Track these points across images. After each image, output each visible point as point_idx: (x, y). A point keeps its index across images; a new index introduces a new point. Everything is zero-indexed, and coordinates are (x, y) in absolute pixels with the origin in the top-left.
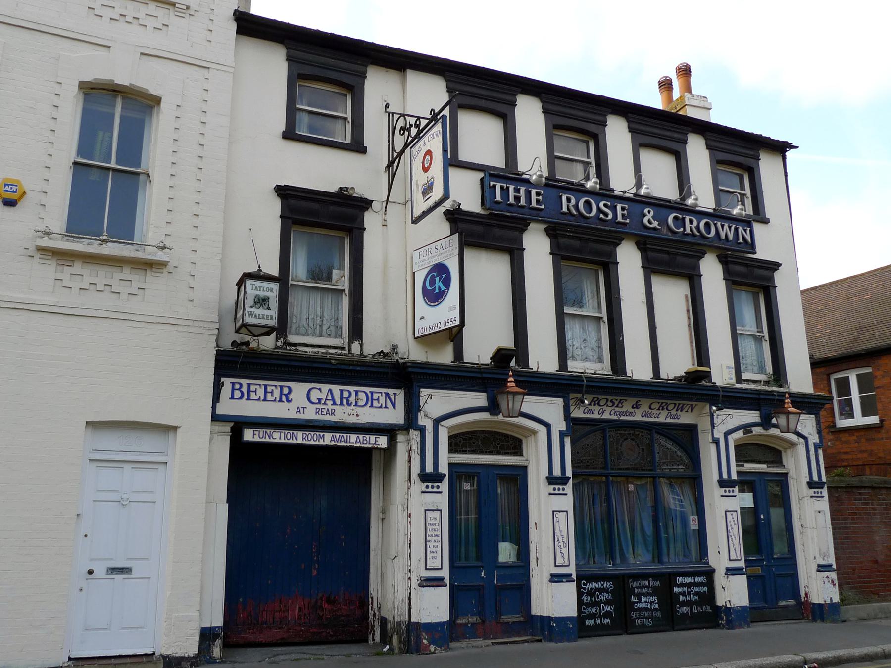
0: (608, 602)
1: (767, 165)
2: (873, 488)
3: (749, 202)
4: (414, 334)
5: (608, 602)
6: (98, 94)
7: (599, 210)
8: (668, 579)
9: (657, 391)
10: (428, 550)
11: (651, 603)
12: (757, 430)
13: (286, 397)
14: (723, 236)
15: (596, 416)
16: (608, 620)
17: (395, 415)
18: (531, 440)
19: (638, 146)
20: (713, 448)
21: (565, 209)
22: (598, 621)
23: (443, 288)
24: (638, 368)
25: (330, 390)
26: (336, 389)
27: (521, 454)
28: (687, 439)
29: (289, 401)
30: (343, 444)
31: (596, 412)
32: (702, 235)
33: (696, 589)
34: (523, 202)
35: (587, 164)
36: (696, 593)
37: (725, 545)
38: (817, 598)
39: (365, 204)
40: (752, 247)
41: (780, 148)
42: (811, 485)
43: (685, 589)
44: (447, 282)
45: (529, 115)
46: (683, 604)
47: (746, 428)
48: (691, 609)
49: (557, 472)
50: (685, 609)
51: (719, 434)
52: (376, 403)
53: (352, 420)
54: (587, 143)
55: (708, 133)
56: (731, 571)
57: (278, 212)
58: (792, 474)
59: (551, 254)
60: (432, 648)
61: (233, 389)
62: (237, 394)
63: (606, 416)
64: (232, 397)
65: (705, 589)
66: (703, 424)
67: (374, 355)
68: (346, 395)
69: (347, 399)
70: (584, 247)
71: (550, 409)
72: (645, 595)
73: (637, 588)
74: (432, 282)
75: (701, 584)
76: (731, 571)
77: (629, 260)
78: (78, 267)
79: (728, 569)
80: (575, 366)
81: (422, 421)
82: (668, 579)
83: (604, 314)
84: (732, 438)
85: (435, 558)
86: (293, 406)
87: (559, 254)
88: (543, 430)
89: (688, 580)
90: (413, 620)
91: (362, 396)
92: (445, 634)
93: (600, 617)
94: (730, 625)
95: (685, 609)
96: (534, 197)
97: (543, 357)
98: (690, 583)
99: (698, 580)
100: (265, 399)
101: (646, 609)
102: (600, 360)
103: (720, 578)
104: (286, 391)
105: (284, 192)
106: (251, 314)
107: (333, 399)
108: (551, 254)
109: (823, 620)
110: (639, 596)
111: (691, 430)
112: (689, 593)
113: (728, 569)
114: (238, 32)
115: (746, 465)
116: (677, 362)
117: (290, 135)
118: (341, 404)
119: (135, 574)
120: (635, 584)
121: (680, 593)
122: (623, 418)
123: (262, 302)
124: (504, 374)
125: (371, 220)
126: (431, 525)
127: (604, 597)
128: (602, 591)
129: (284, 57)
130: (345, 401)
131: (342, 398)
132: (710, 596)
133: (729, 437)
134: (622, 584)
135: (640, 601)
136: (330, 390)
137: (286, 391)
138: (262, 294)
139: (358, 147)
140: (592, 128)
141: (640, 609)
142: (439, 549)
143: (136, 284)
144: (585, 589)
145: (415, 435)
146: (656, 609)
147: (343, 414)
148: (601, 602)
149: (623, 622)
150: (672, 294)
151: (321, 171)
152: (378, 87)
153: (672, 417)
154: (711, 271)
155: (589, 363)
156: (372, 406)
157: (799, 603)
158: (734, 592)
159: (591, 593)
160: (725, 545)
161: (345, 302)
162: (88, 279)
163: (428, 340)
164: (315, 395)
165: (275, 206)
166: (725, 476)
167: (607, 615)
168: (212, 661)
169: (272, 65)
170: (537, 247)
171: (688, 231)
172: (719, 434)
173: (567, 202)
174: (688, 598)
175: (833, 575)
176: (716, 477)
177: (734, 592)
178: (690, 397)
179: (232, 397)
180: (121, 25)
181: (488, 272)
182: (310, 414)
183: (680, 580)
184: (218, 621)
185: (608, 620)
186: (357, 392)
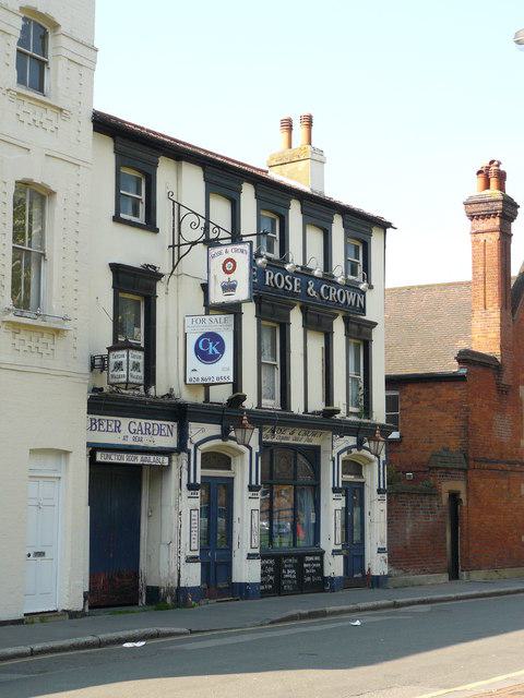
0: (272, 574)
1: (376, 239)
4: (185, 381)
6: (24, 186)
8: (301, 557)
9: (308, 422)
12: (354, 451)
13: (118, 429)
17: (170, 441)
18: (239, 458)
21: (267, 283)
26: (143, 421)
27: (230, 469)
28: (314, 455)
37: (331, 536)
38: (376, 572)
39: (159, 276)
40: (363, 310)
41: (384, 226)
44: (221, 348)
46: (308, 575)
47: (348, 449)
49: (254, 483)
50: (309, 579)
53: (151, 445)
55: (118, 138)
56: (335, 552)
58: (368, 483)
66: (325, 446)
67: (163, 397)
74: (206, 345)
76: (335, 552)
77: (296, 318)
78: (23, 335)
79: (334, 551)
81: (190, 447)
82: (301, 557)
83: (278, 363)
86: (121, 435)
88: (247, 451)
89: (311, 558)
90: (182, 585)
91: (156, 427)
92: (199, 594)
94: (333, 590)
95: (309, 579)
102: (273, 398)
103: (328, 558)
105: (117, 269)
106: (112, 376)
109: (378, 587)
111: (316, 451)
113: (334, 551)
114: (94, 130)
116: (317, 404)
117: (117, 219)
119: (47, 556)
124: (230, 415)
125: (160, 288)
129: (112, 150)
130: (148, 431)
132: (320, 571)
134: (278, 558)
139: (150, 225)
145: (184, 455)
147: (147, 441)
151: (138, 249)
152: (165, 172)
154: (339, 327)
157: (364, 576)
158: (334, 567)
160: (331, 536)
163: (191, 386)
164: (133, 427)
165: (108, 278)
166: (192, 481)
169: (102, 158)
175: (386, 555)
176: (331, 486)
177: (334, 567)
178: (322, 427)
182: (130, 442)
183: (308, 558)
184: (87, 590)
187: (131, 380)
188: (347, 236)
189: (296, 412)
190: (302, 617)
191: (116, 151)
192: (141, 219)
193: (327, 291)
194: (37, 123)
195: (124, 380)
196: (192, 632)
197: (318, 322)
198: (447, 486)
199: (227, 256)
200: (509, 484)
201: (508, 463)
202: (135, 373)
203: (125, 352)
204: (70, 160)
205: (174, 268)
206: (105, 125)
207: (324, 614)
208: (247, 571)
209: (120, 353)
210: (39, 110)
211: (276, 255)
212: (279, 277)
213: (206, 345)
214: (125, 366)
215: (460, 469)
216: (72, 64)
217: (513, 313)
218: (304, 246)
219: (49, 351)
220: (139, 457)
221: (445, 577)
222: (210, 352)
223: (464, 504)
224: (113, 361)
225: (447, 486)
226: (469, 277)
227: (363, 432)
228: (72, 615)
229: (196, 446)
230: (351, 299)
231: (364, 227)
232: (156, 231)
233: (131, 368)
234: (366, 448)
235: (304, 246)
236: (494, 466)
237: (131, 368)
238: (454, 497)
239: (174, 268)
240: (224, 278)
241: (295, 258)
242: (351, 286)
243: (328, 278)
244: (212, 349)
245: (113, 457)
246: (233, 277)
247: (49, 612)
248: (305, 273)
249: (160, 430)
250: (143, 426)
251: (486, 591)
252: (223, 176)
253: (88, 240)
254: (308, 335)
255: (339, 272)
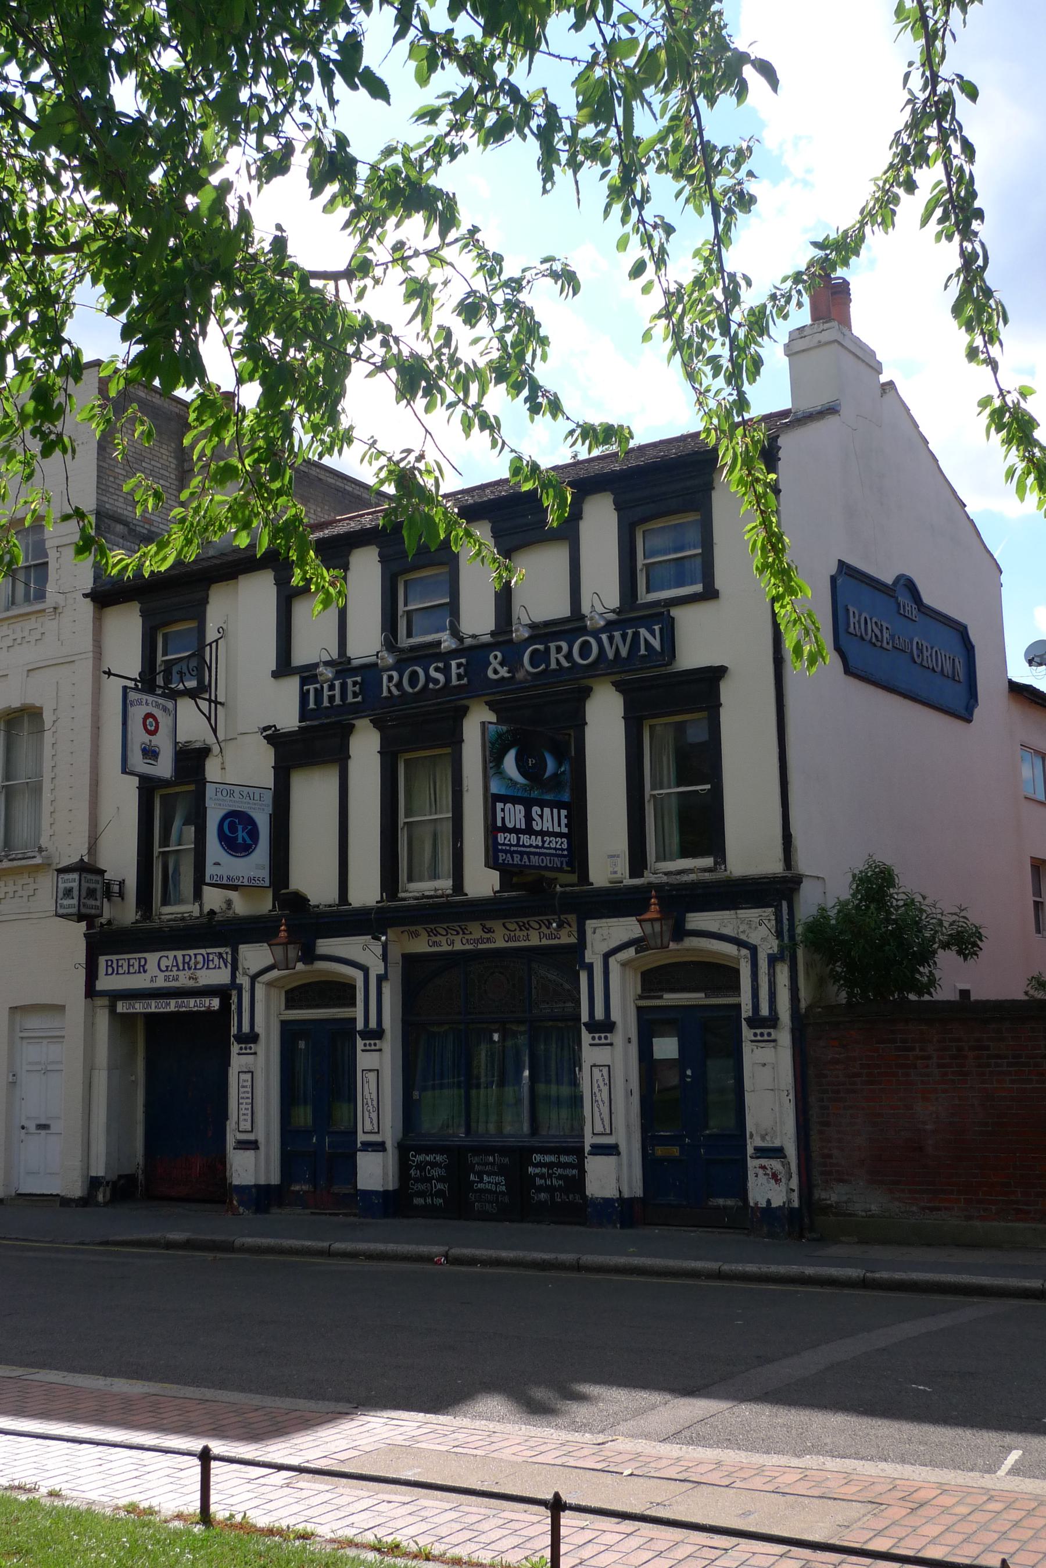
0: (440, 1179)
3: (262, 853)
5: (440, 1179)
10: (241, 1112)
11: (496, 1184)
14: (610, 654)
15: (445, 948)
16: (441, 1201)
22: (429, 1201)
23: (249, 841)
25: (175, 956)
26: (179, 954)
29: (145, 972)
30: (184, 1009)
31: (444, 942)
33: (560, 1171)
34: (338, 701)
36: (560, 1177)
43: (545, 1170)
46: (540, 1189)
48: (552, 1197)
50: (543, 1196)
52: (211, 965)
59: (779, 459)
60: (241, 1209)
61: (107, 966)
62: (110, 970)
63: (458, 946)
64: (107, 974)
65: (575, 1172)
68: (187, 959)
69: (188, 963)
72: (489, 1174)
73: (478, 1164)
74: (233, 828)
75: (566, 1166)
85: (246, 1120)
86: (147, 976)
88: (358, 976)
89: (549, 1158)
91: (200, 958)
93: (431, 1195)
95: (543, 1196)
96: (350, 688)
98: (552, 1162)
99: (564, 1159)
100: (129, 973)
101: (490, 1191)
104: (143, 963)
107: (177, 965)
108: (779, 459)
110: (480, 1175)
112: (550, 1176)
115: (666, 996)
118: (184, 969)
120: (476, 1160)
121: (536, 1175)
122: (481, 946)
126: (243, 1087)
127: (436, 1172)
128: (434, 1165)
131: (184, 963)
132: (578, 1182)
133: (612, 960)
135: (481, 1181)
136: (175, 956)
137: (143, 963)
141: (481, 1191)
142: (249, 1112)
144: (413, 1161)
146: (502, 1192)
148: (432, 1178)
149: (458, 1205)
153: (551, 937)
156: (208, 968)
159: (421, 1167)
167: (440, 1193)
168: (97, 1204)
171: (553, 665)
174: (549, 1183)
179: (107, 974)
182: (160, 983)
183: (537, 1158)
185: (441, 1201)
186: (195, 955)
202: (66, 902)
213: (233, 828)
220: (173, 1002)
222: (240, 840)
228: (65, 1202)
229: (254, 978)
244: (241, 835)
245: (137, 1006)
246: (156, 740)
247: (51, 1195)
249: (207, 961)
250: (180, 959)
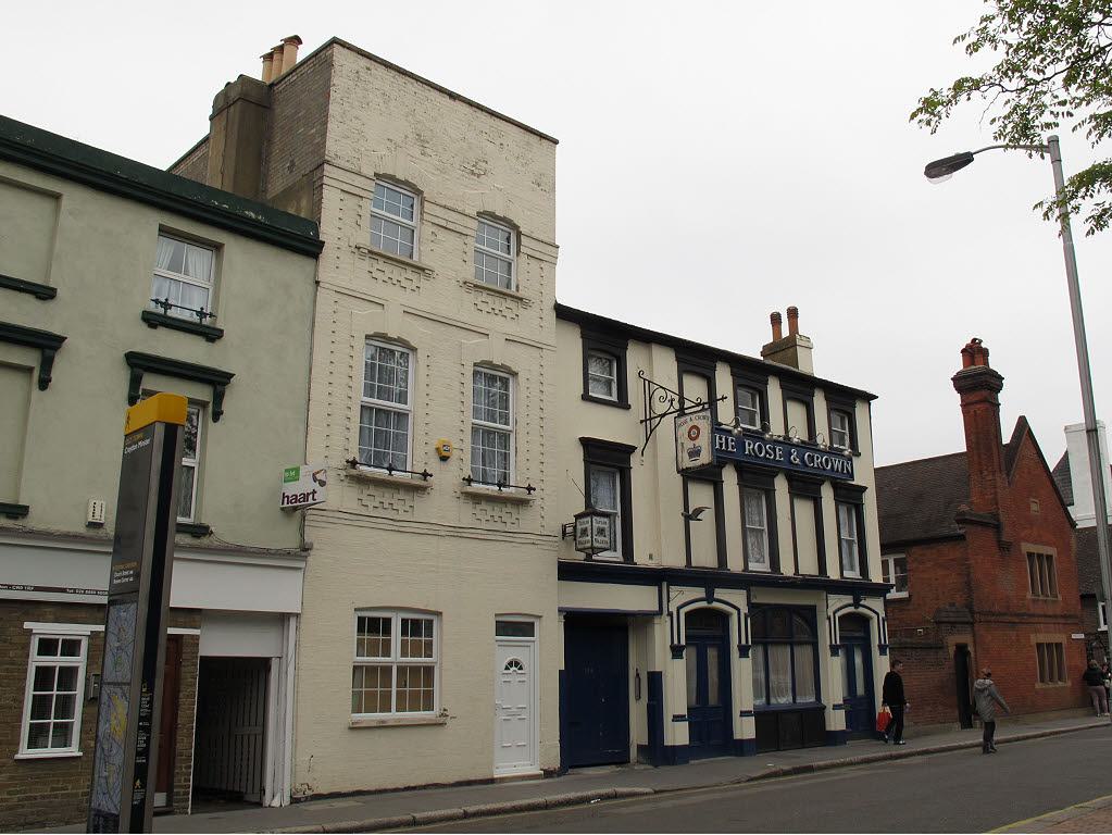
1: (860, 410)
2: (912, 648)
7: (767, 452)
19: (786, 399)
20: (668, 619)
24: (787, 569)
28: (809, 615)
32: (756, 456)
35: (609, 383)
40: (852, 476)
41: (868, 398)
42: (880, 646)
45: (724, 379)
49: (743, 642)
51: (673, 609)
54: (611, 362)
57: (736, 481)
70: (756, 478)
71: (737, 598)
77: (781, 486)
78: (484, 505)
80: (753, 566)
84: (683, 611)
87: (742, 483)
88: (735, 612)
96: (730, 444)
97: (735, 564)
111: (812, 609)
114: (557, 317)
117: (586, 397)
123: (601, 531)
125: (635, 460)
138: (601, 526)
139: (622, 403)
140: (806, 399)
143: (408, 503)
150: (804, 510)
151: (611, 427)
152: (635, 357)
154: (827, 493)
155: (760, 566)
158: (836, 721)
161: (766, 537)
162: (490, 513)
166: (676, 642)
169: (571, 343)
170: (730, 478)
172: (673, 609)
173: (750, 447)
176: (828, 643)
180: (492, 316)
181: (701, 496)
187: (596, 545)
188: (830, 410)
189: (832, 578)
190: (786, 773)
191: (678, 360)
192: (614, 398)
193: (811, 459)
194: (497, 312)
195: (589, 545)
196: (656, 792)
197: (805, 486)
198: (953, 640)
199: (691, 424)
200: (1017, 636)
201: (1018, 615)
202: (600, 538)
203: (589, 519)
204: (472, 328)
205: (647, 440)
206: (564, 314)
207: (810, 769)
208: (745, 729)
209: (585, 520)
210: (497, 300)
211: (758, 427)
212: (759, 446)
214: (589, 532)
215: (967, 623)
216: (533, 260)
217: (1008, 475)
218: (785, 419)
219: (408, 508)
221: (957, 725)
223: (972, 655)
224: (579, 527)
225: (953, 640)
226: (961, 446)
227: (860, 589)
230: (837, 465)
231: (846, 401)
232: (628, 407)
233: (595, 532)
234: (864, 606)
235: (785, 419)
236: (1001, 619)
237: (595, 532)
238: (961, 650)
239: (647, 440)
240: (689, 445)
241: (776, 429)
242: (833, 452)
243: (810, 444)
246: (697, 443)
248: (786, 442)
251: (1020, 735)
252: (696, 358)
253: (557, 412)
254: (795, 501)
255: (823, 438)
